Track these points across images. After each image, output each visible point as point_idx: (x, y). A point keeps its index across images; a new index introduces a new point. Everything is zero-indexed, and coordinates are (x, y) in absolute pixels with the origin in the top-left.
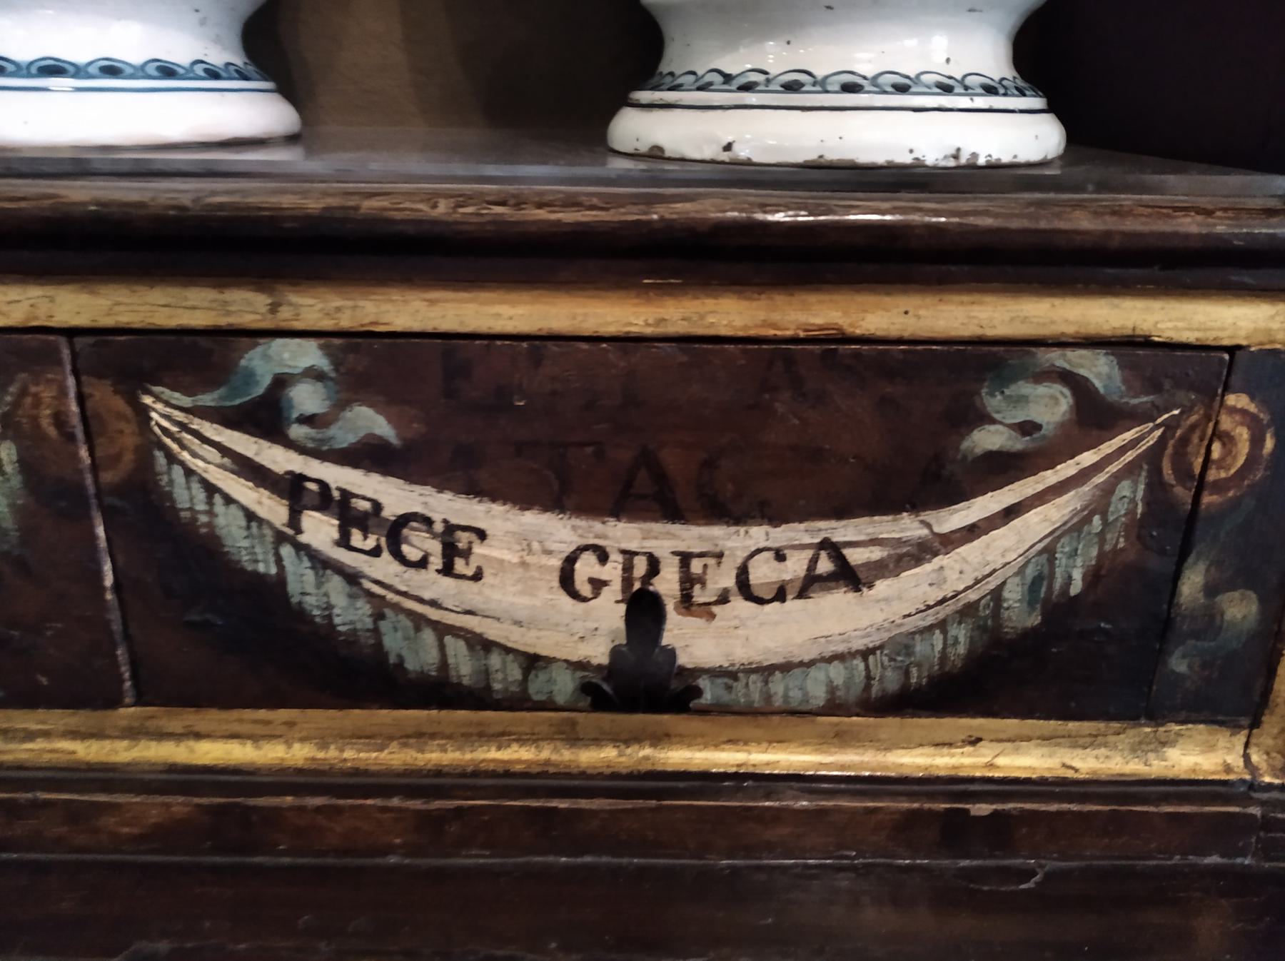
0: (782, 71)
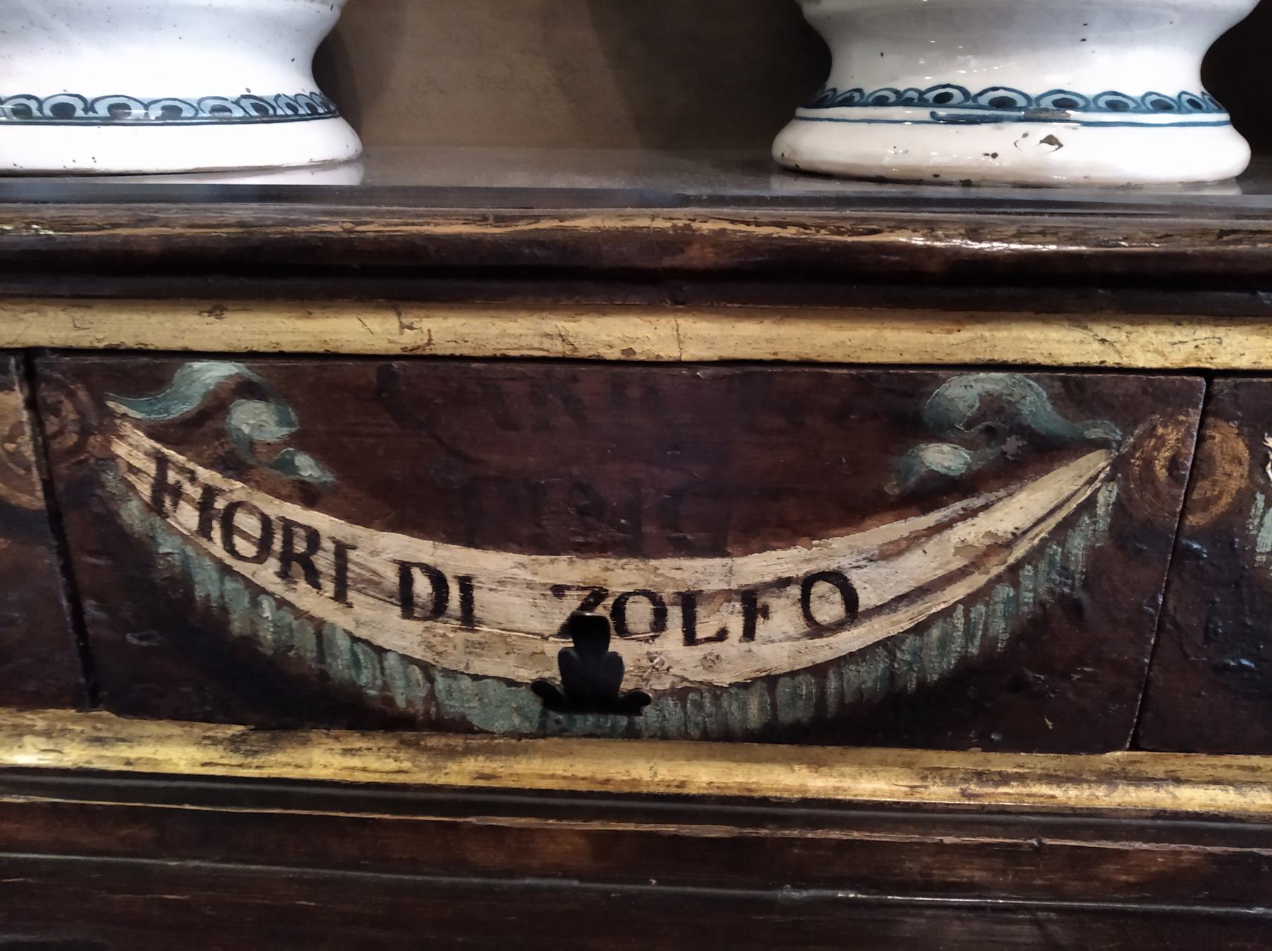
0: (173, 97)
